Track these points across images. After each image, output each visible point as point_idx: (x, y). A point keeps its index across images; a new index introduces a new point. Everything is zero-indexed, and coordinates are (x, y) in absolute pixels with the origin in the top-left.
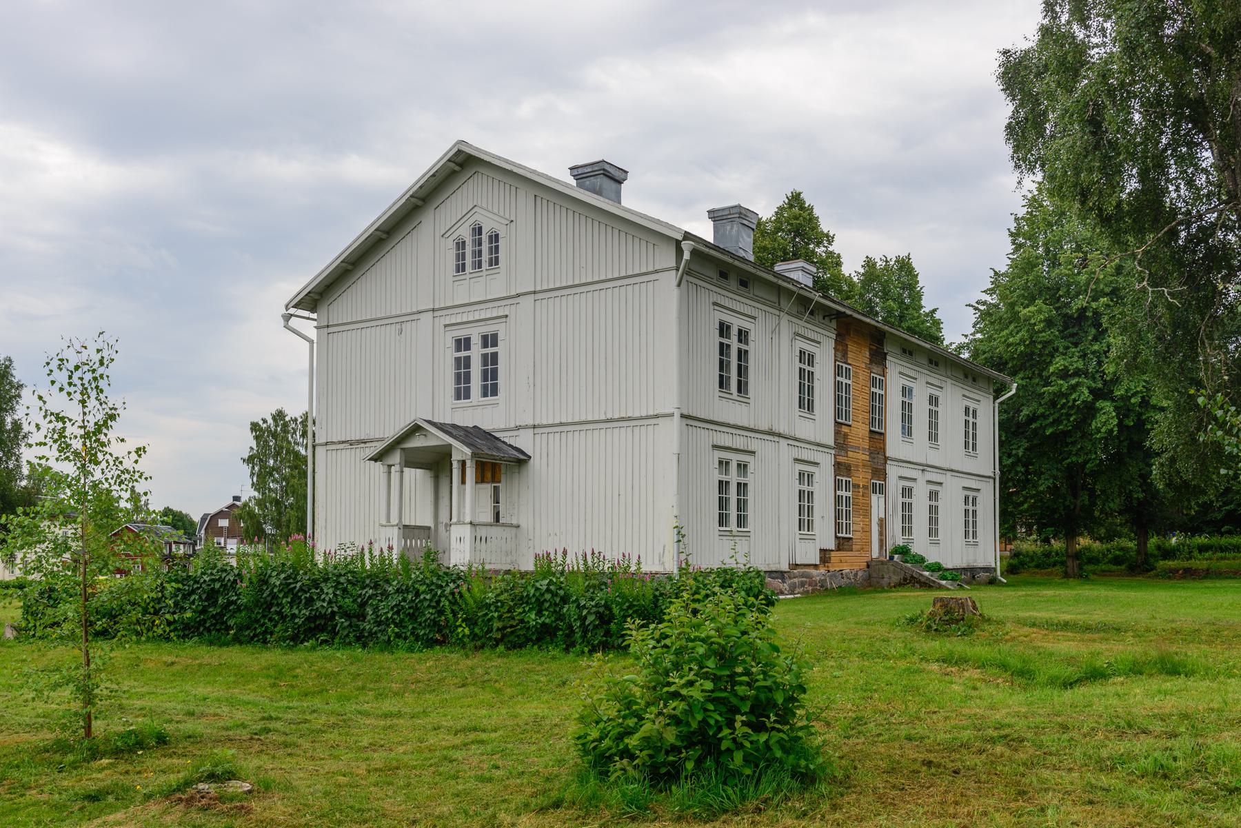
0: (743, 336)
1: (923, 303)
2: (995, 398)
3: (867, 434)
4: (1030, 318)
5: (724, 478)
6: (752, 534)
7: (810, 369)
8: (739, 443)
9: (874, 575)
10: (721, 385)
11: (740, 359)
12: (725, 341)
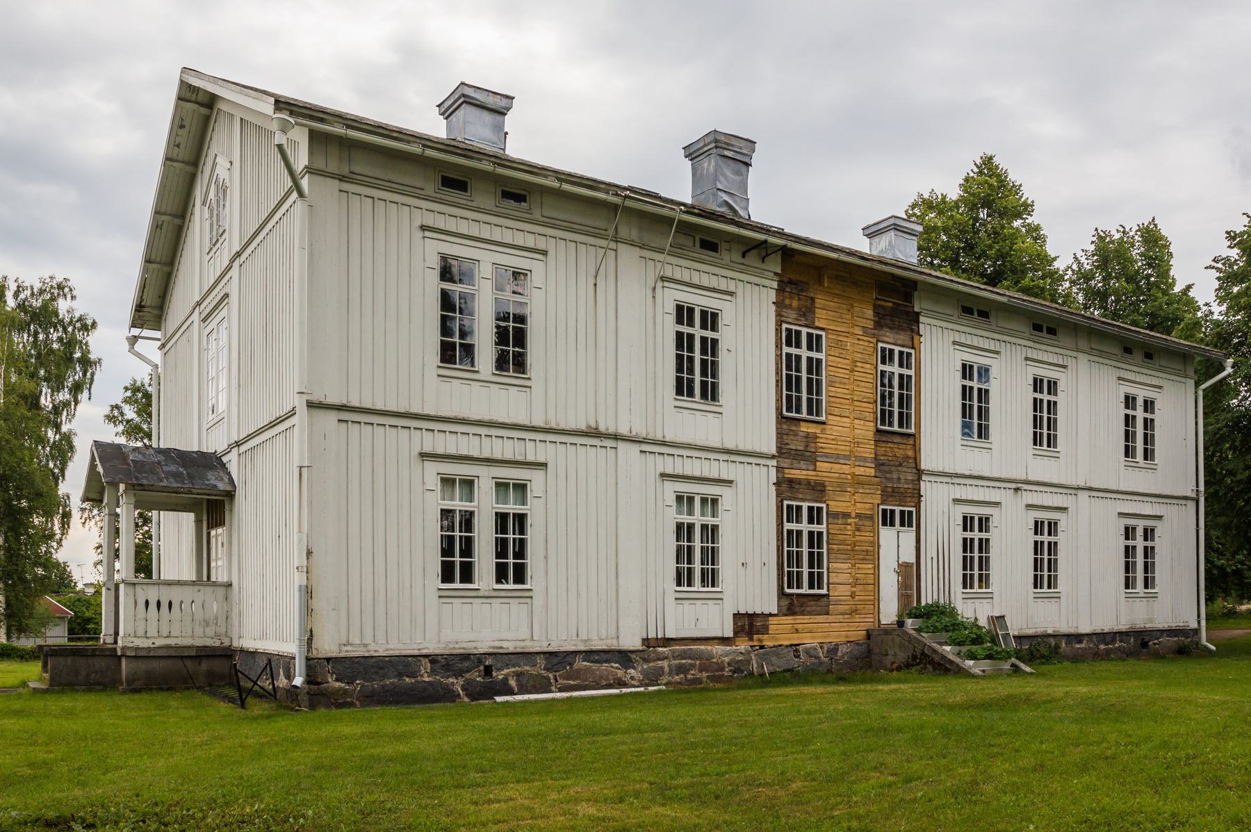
0: (1149, 405)
1: (1051, 249)
2: (1197, 385)
3: (870, 435)
5: (686, 519)
6: (995, 596)
7: (1052, 398)
8: (1147, 509)
9: (877, 650)
10: (1127, 455)
11: (1146, 428)
12: (1130, 412)
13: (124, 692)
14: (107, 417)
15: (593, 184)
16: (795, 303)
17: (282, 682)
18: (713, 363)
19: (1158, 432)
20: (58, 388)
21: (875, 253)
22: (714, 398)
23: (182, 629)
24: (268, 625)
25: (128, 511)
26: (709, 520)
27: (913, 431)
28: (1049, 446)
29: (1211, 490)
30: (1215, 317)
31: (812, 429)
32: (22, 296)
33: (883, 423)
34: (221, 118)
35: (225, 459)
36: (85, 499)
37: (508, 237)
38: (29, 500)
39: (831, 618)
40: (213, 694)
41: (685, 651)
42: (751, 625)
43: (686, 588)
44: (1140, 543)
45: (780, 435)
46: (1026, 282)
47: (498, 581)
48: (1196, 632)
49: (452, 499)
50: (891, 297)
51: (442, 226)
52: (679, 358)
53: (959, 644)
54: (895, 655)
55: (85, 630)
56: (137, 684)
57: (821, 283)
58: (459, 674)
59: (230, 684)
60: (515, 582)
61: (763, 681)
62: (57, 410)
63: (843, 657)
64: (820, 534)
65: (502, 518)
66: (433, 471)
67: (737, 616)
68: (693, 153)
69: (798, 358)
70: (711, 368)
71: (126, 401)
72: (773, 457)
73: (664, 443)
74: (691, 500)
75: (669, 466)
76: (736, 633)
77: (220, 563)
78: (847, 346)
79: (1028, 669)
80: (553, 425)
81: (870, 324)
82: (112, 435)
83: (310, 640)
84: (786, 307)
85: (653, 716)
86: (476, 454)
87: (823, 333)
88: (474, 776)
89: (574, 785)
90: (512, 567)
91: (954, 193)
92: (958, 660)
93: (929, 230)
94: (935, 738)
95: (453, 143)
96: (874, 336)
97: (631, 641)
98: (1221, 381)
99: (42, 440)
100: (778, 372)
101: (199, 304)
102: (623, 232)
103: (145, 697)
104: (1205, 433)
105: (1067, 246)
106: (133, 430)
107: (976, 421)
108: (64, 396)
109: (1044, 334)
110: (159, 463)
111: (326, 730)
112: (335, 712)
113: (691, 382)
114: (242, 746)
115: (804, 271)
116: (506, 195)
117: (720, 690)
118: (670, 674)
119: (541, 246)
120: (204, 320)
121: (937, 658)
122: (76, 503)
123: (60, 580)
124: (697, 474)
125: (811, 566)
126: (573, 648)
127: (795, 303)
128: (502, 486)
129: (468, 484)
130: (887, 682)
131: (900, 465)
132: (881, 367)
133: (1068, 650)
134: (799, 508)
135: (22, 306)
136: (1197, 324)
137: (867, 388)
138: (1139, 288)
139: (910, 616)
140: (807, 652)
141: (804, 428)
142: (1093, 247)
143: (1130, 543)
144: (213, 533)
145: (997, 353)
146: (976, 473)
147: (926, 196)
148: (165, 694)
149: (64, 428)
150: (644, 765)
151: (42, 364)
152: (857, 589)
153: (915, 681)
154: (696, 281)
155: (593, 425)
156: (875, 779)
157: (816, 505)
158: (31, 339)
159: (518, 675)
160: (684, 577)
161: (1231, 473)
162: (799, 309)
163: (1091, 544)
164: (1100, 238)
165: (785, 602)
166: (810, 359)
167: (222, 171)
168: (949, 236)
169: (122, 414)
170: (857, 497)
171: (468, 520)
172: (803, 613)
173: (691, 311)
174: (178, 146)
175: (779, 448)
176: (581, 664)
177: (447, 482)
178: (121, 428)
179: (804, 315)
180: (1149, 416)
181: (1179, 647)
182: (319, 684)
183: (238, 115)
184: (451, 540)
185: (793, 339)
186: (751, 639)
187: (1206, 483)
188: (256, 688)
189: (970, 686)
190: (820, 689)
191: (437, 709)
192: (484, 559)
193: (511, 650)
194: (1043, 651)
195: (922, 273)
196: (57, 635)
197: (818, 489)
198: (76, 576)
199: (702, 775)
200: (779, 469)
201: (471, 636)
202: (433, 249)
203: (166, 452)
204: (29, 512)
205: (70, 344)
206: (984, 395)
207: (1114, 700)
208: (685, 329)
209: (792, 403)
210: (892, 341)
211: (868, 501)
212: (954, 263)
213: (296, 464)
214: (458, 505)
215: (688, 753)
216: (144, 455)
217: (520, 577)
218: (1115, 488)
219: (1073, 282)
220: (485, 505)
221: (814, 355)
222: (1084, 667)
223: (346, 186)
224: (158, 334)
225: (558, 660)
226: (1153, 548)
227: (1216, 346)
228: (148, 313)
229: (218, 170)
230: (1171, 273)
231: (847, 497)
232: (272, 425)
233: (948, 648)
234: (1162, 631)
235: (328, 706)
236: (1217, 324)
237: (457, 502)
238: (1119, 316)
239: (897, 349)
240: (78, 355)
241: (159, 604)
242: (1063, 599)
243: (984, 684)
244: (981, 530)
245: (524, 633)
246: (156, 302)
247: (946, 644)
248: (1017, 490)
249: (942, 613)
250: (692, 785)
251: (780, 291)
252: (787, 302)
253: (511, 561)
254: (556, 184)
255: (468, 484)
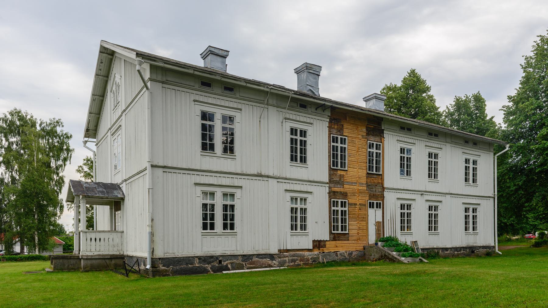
0: (475, 162)
1: (437, 104)
2: (495, 154)
3: (365, 175)
4: (525, 108)
5: (294, 206)
7: (436, 160)
9: (367, 254)
10: (466, 181)
12: (467, 165)
13: (82, 272)
14: (77, 170)
15: (259, 84)
16: (336, 127)
17: (142, 267)
18: (305, 149)
19: (478, 172)
20: (58, 159)
21: (368, 107)
22: (305, 162)
23: (105, 248)
24: (137, 247)
25: (83, 205)
26: (303, 206)
27: (381, 173)
28: (435, 178)
29: (500, 194)
30: (503, 129)
31: (342, 173)
32: (43, 126)
33: (369, 170)
34: (117, 60)
35: (121, 186)
36: (67, 201)
37: (227, 104)
38: (47, 202)
39: (350, 242)
40: (116, 272)
41: (294, 254)
42: (319, 244)
43: (295, 231)
44: (471, 214)
46: (427, 117)
47: (224, 229)
48: (494, 247)
49: (207, 200)
50: (373, 124)
51: (201, 100)
52: (292, 147)
53: (399, 251)
54: (374, 255)
55: (69, 249)
56: (87, 269)
57: (346, 119)
58: (209, 263)
59: (123, 268)
61: (324, 265)
62: (57, 168)
64: (345, 211)
65: (225, 207)
66: (199, 189)
67: (314, 241)
68: (298, 71)
69: (337, 147)
70: (303, 151)
71: (84, 164)
72: (327, 183)
73: (286, 179)
74: (296, 199)
75: (288, 187)
76: (314, 247)
77: (119, 224)
78: (355, 141)
79: (426, 261)
80: (244, 173)
81: (365, 134)
82: (78, 177)
83: (153, 252)
84: (332, 128)
85: (281, 278)
86: (215, 183)
88: (212, 301)
89: (248, 304)
90: (229, 224)
91: (399, 84)
92: (398, 257)
93: (389, 98)
94: (386, 287)
95: (206, 69)
96: (366, 138)
97: (274, 250)
98: (504, 153)
99: (51, 179)
100: (329, 152)
101: (110, 129)
102: (271, 102)
103: (90, 273)
104: (498, 173)
105: (444, 103)
106: (87, 175)
107: (406, 169)
108: (60, 162)
109: (433, 136)
110: (95, 188)
111: (157, 285)
112: (162, 278)
113: (296, 156)
114: (125, 291)
115: (340, 115)
116: (226, 88)
117: (308, 268)
118: (289, 262)
119: (239, 107)
120: (112, 135)
121: (390, 257)
122: (65, 204)
123: (60, 231)
124: (299, 190)
125: (342, 223)
126: (252, 253)
127: (336, 127)
128: (225, 195)
129: (212, 194)
130: (371, 265)
132: (369, 150)
133: (442, 254)
134: (337, 202)
135: (43, 129)
136: (495, 132)
137: (363, 157)
138: (472, 118)
139: (380, 241)
140: (341, 254)
141: (339, 172)
142: (454, 103)
143: (467, 214)
144: (117, 213)
145: (414, 144)
147: (388, 85)
148: (98, 272)
149: (60, 175)
150: (276, 296)
151: (51, 151)
152: (360, 231)
153: (382, 265)
154: (298, 119)
155: (260, 172)
156: (362, 301)
157: (344, 201)
158: (47, 142)
159: (232, 263)
160: (293, 227)
161: (509, 187)
162: (337, 129)
163: (451, 215)
164: (457, 100)
166: (341, 147)
167: (117, 79)
168: (397, 100)
169: (83, 169)
170: (360, 198)
172: (339, 240)
173: (296, 130)
174: (100, 70)
175: (330, 180)
176: (255, 259)
177: (205, 193)
178: (82, 174)
179: (339, 131)
180: (475, 166)
181: (488, 253)
182: (156, 268)
183: (123, 58)
184: (206, 214)
185: (335, 140)
186: (319, 250)
187: (498, 191)
188: (132, 269)
189: (403, 267)
190: (344, 268)
191: (200, 276)
193: (229, 254)
194: (433, 254)
195: (385, 115)
196: (58, 251)
197: (345, 195)
198: (66, 229)
199: (297, 300)
200: (330, 188)
201: (214, 249)
202: (198, 109)
203: (98, 184)
204: (47, 206)
205: (62, 143)
206: (409, 159)
207: (458, 273)
208: (294, 137)
209: (335, 164)
210: (373, 140)
211: (365, 199)
212: (399, 110)
213: (147, 187)
214: (209, 202)
215: (293, 292)
216: (89, 185)
217: (232, 227)
218: (461, 194)
219: (446, 117)
220: (219, 202)
221: (343, 146)
222: (448, 260)
223: (164, 85)
224: (95, 140)
225: (247, 258)
226: (410, 213)
227: (503, 140)
228: (91, 132)
229: (116, 79)
230: (486, 112)
231: (355, 197)
232: (138, 173)
233: (395, 253)
234: (480, 247)
235: (159, 276)
236: (503, 131)
237: (208, 201)
238: (464, 129)
239: (375, 143)
240: (65, 147)
241: (96, 239)
242: (440, 235)
243: (408, 266)
244: (407, 209)
245: (234, 248)
246: (94, 128)
247: (394, 251)
249: (393, 240)
250: (293, 304)
251: (330, 122)
253: (229, 222)
254: (244, 84)
255: (212, 194)
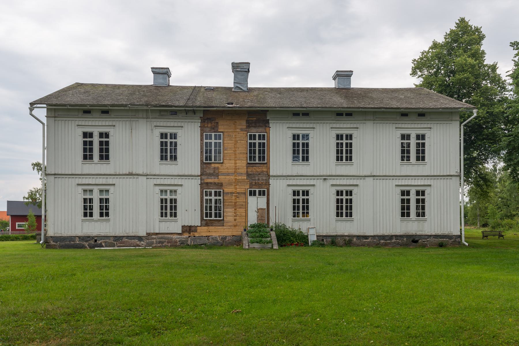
2: (461, 123)
5: (164, 197)
16: (209, 125)
26: (173, 197)
31: (217, 165)
45: (202, 168)
58: (87, 241)
60: (422, 216)
61: (188, 246)
63: (229, 240)
65: (101, 200)
66: (80, 188)
67: (183, 227)
72: (198, 176)
73: (155, 175)
87: (222, 134)
90: (105, 212)
96: (246, 131)
97: (142, 233)
118: (156, 243)
128: (101, 191)
129: (91, 191)
131: (259, 174)
140: (212, 238)
141: (213, 165)
146: (300, 174)
165: (204, 222)
171: (91, 200)
172: (212, 226)
176: (125, 240)
179: (213, 129)
192: (96, 211)
193: (103, 235)
220: (96, 197)
225: (118, 239)
231: (233, 187)
234: (430, 236)
248: (325, 179)
252: (206, 125)
255: (91, 191)
